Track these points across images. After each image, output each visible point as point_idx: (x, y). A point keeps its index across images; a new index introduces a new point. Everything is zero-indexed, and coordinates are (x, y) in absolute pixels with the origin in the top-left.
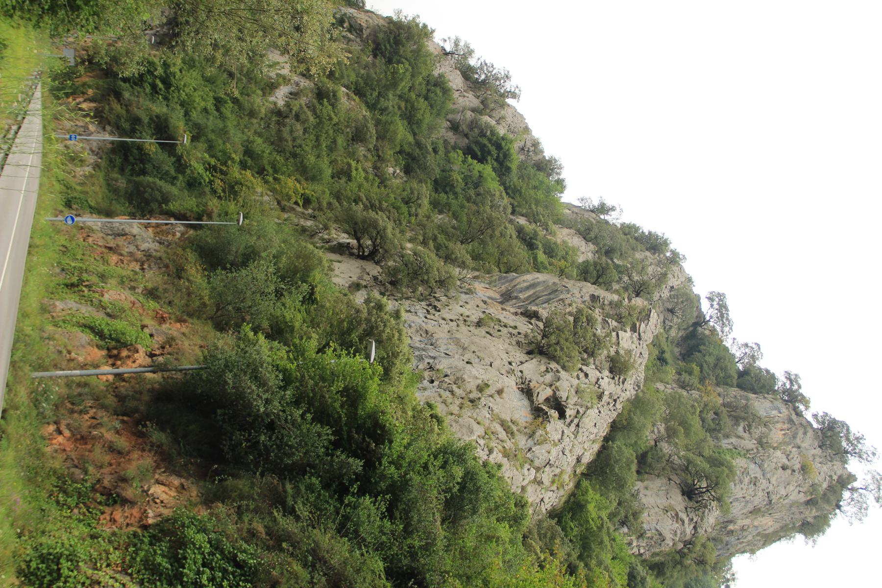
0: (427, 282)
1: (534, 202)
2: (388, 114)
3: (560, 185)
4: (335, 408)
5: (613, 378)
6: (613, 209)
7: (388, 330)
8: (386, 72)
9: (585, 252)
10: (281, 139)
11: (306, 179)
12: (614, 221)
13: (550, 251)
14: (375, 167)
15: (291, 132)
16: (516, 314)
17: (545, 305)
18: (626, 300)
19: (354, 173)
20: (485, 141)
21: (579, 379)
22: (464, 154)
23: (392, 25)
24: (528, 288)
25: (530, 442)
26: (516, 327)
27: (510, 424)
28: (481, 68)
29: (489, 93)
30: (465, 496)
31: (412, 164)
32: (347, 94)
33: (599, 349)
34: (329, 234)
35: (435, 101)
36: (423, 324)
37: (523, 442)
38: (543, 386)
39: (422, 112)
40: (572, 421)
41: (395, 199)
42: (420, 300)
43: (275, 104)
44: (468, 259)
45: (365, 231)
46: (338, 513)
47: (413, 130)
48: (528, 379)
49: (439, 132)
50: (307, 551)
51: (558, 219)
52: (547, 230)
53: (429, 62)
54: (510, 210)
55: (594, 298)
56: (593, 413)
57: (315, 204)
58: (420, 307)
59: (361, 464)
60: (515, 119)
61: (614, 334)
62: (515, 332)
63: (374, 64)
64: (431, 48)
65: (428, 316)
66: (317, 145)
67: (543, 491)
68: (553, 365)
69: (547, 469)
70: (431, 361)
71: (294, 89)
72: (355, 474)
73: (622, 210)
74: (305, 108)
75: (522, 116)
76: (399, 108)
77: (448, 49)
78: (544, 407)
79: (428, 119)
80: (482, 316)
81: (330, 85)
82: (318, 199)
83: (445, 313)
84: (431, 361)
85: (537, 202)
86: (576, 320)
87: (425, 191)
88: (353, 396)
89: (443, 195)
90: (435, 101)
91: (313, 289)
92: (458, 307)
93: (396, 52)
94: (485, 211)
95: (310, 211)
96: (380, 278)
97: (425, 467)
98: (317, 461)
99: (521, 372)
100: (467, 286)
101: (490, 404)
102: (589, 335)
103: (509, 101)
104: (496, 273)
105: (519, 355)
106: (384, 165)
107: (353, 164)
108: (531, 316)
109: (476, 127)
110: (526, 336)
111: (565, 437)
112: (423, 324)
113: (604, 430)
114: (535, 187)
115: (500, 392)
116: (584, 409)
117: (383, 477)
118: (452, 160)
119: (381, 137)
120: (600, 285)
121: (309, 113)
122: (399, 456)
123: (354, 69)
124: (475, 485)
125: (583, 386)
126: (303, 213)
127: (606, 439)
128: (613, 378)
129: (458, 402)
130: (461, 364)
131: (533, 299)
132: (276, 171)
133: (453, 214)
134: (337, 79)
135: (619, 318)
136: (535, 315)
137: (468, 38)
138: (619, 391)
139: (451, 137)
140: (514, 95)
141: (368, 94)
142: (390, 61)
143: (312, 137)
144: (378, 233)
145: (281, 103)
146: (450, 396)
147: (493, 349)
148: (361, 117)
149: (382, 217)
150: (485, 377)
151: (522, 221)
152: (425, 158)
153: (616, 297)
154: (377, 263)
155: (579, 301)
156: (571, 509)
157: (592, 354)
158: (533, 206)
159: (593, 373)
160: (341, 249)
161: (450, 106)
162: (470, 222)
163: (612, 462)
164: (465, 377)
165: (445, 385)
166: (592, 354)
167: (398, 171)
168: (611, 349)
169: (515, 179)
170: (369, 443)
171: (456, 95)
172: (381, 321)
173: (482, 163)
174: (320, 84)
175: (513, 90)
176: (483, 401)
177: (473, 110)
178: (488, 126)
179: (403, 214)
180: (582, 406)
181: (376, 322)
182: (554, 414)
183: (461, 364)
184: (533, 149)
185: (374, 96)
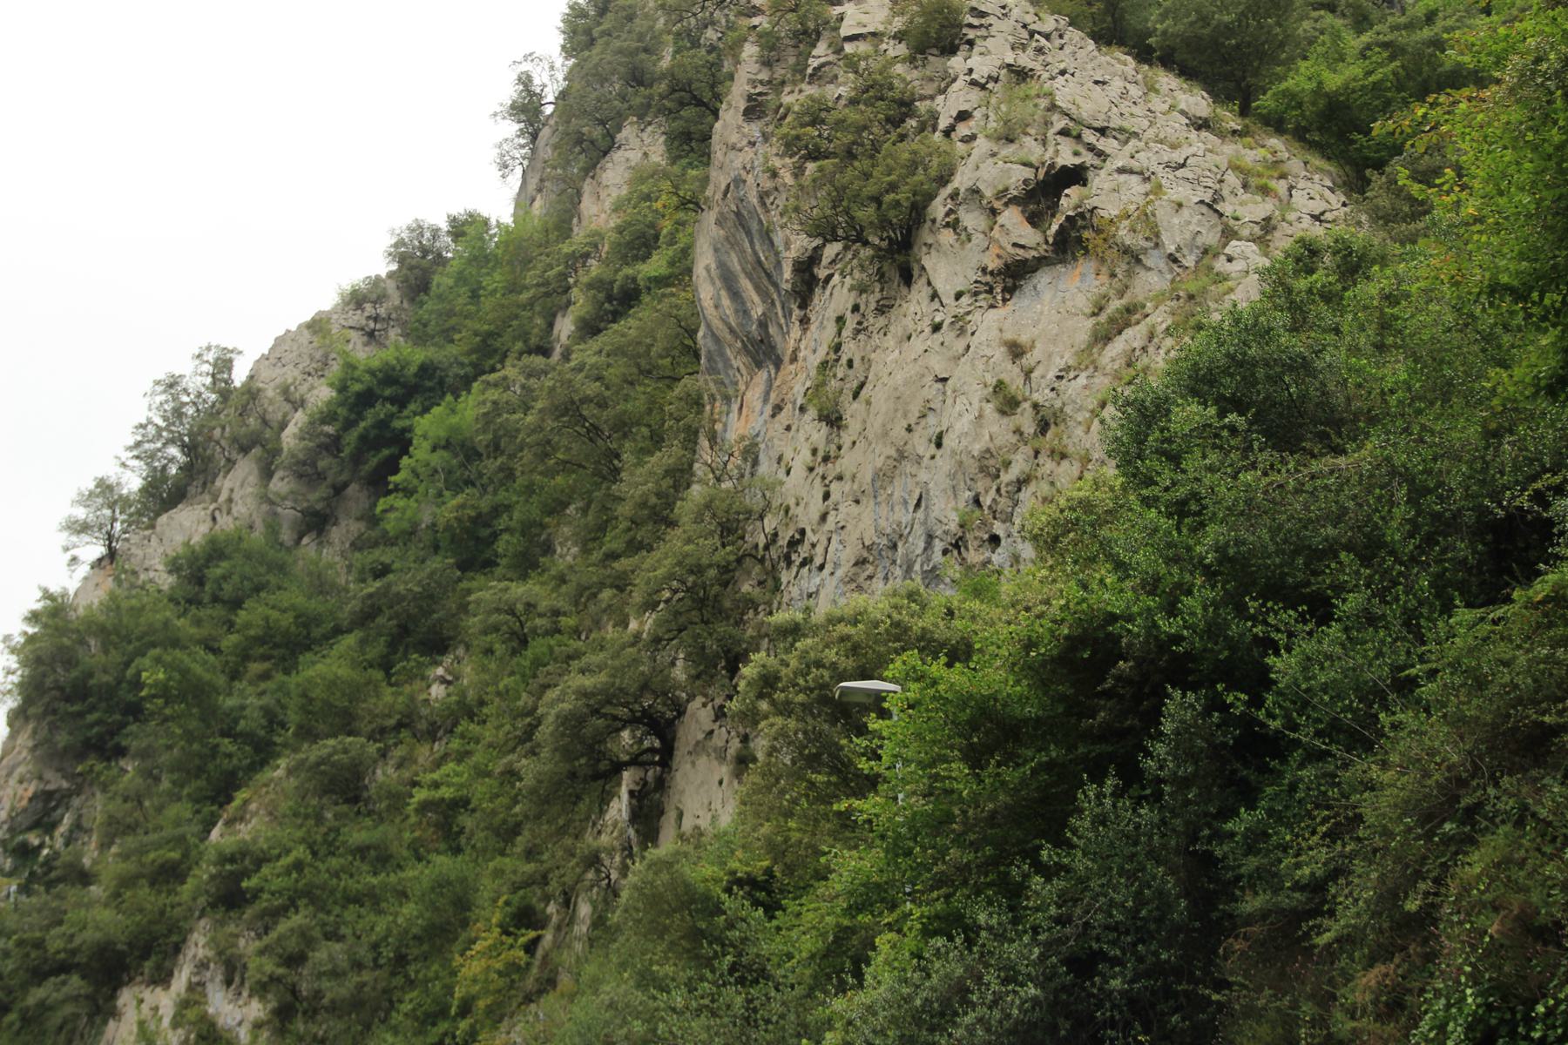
0: (725, 569)
1: (513, 297)
2: (284, 707)
3: (466, 228)
4: (1024, 782)
5: (971, 43)
6: (525, 81)
7: (831, 655)
8: (166, 720)
9: (641, 148)
10: (356, 1003)
11: (465, 924)
12: (560, 76)
13: (641, 243)
14: (432, 735)
15: (335, 974)
16: (805, 321)
17: (778, 239)
18: (755, 21)
19: (446, 793)
20: (352, 437)
21: (973, 137)
22: (389, 492)
23: (32, 711)
24: (735, 295)
25: (1153, 259)
26: (840, 320)
27: (1103, 318)
28: (152, 456)
29: (217, 432)
30: (1258, 394)
31: (419, 634)
32: (229, 823)
33: (891, 88)
34: (610, 852)
35: (244, 578)
36: (839, 573)
37: (1153, 278)
38: (996, 233)
39: (275, 614)
40: (1091, 148)
41: (512, 673)
42: (777, 588)
43: (258, 1026)
44: (660, 460)
45: (594, 748)
46: (1323, 756)
47: (326, 637)
48: (979, 276)
49: (330, 566)
50: (1428, 836)
51: (558, 227)
52: (587, 256)
53: (134, 602)
54: (538, 361)
55: (754, 110)
56: (1065, 93)
57: (534, 896)
58: (796, 583)
59: (1178, 694)
60: (288, 357)
61: (849, 48)
62: (851, 323)
63: (144, 754)
64: (97, 597)
65: (818, 561)
66: (371, 899)
67: (1292, 216)
68: (938, 209)
69: (1226, 208)
70: (938, 546)
71: (216, 974)
72: (1207, 712)
73: (528, 57)
74: (266, 940)
75: (279, 341)
76: (265, 676)
77: (97, 550)
78: (1055, 227)
79: (294, 596)
80: (812, 413)
81: (204, 872)
82: (515, 888)
83: (807, 516)
84: (938, 546)
85: (514, 288)
86: (815, 155)
87: (490, 592)
88: (986, 732)
89: (501, 546)
90: (244, 578)
91: (740, 882)
92: (791, 482)
93: (108, 693)
94: (539, 428)
95: (551, 909)
96: (718, 701)
97: (1179, 510)
98: (1177, 822)
99: (958, 296)
100: (737, 460)
101: (1051, 375)
102: (853, 116)
103: (239, 376)
104: (702, 382)
105: (915, 303)
106: (424, 711)
107: (420, 795)
108: (807, 280)
109: (314, 465)
110: (862, 289)
111: (1134, 164)
112: (839, 573)
113: (1120, 63)
114: (475, 296)
115: (1016, 351)
116: (1055, 117)
117: (1214, 630)
118: (405, 525)
119: (346, 723)
120: (718, 98)
121: (283, 926)
122: (1152, 593)
123: (160, 809)
124: (1226, 372)
125: (992, 125)
126: (558, 928)
127: (1144, 55)
128: (971, 43)
129: (1048, 465)
130: (944, 463)
131: (764, 275)
132: (443, 1013)
133: (550, 513)
134: (186, 855)
135: (807, 37)
136: (806, 269)
137: (64, 499)
138: (1006, 26)
139: (345, 530)
140: (223, 364)
141: (227, 765)
142: (135, 711)
143: (350, 913)
144: (595, 712)
145: (256, 1009)
146: (1032, 487)
147: (899, 377)
148: (293, 782)
149: (552, 704)
150: (976, 393)
151: (565, 327)
152: (400, 598)
153: (750, 50)
154: (680, 711)
155: (762, 148)
156: (1342, 136)
157: (906, 106)
158: (525, 296)
159: (958, 98)
160: (648, 814)
161: (258, 536)
162: (566, 466)
163: (1206, 31)
164: (977, 449)
165: (1004, 503)
166: (906, 106)
167: (440, 671)
168: (891, 53)
169: (453, 350)
170: (1118, 678)
171: (226, 523)
172: (805, 675)
173: (410, 442)
174: (202, 901)
175: (207, 368)
176: (1042, 396)
177: (267, 473)
178: (306, 433)
179: (551, 649)
180: (1048, 124)
181: (807, 690)
182: (1071, 198)
183: (944, 463)
184: (368, 306)
185: (232, 748)
